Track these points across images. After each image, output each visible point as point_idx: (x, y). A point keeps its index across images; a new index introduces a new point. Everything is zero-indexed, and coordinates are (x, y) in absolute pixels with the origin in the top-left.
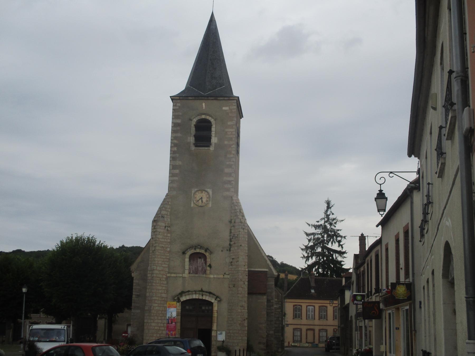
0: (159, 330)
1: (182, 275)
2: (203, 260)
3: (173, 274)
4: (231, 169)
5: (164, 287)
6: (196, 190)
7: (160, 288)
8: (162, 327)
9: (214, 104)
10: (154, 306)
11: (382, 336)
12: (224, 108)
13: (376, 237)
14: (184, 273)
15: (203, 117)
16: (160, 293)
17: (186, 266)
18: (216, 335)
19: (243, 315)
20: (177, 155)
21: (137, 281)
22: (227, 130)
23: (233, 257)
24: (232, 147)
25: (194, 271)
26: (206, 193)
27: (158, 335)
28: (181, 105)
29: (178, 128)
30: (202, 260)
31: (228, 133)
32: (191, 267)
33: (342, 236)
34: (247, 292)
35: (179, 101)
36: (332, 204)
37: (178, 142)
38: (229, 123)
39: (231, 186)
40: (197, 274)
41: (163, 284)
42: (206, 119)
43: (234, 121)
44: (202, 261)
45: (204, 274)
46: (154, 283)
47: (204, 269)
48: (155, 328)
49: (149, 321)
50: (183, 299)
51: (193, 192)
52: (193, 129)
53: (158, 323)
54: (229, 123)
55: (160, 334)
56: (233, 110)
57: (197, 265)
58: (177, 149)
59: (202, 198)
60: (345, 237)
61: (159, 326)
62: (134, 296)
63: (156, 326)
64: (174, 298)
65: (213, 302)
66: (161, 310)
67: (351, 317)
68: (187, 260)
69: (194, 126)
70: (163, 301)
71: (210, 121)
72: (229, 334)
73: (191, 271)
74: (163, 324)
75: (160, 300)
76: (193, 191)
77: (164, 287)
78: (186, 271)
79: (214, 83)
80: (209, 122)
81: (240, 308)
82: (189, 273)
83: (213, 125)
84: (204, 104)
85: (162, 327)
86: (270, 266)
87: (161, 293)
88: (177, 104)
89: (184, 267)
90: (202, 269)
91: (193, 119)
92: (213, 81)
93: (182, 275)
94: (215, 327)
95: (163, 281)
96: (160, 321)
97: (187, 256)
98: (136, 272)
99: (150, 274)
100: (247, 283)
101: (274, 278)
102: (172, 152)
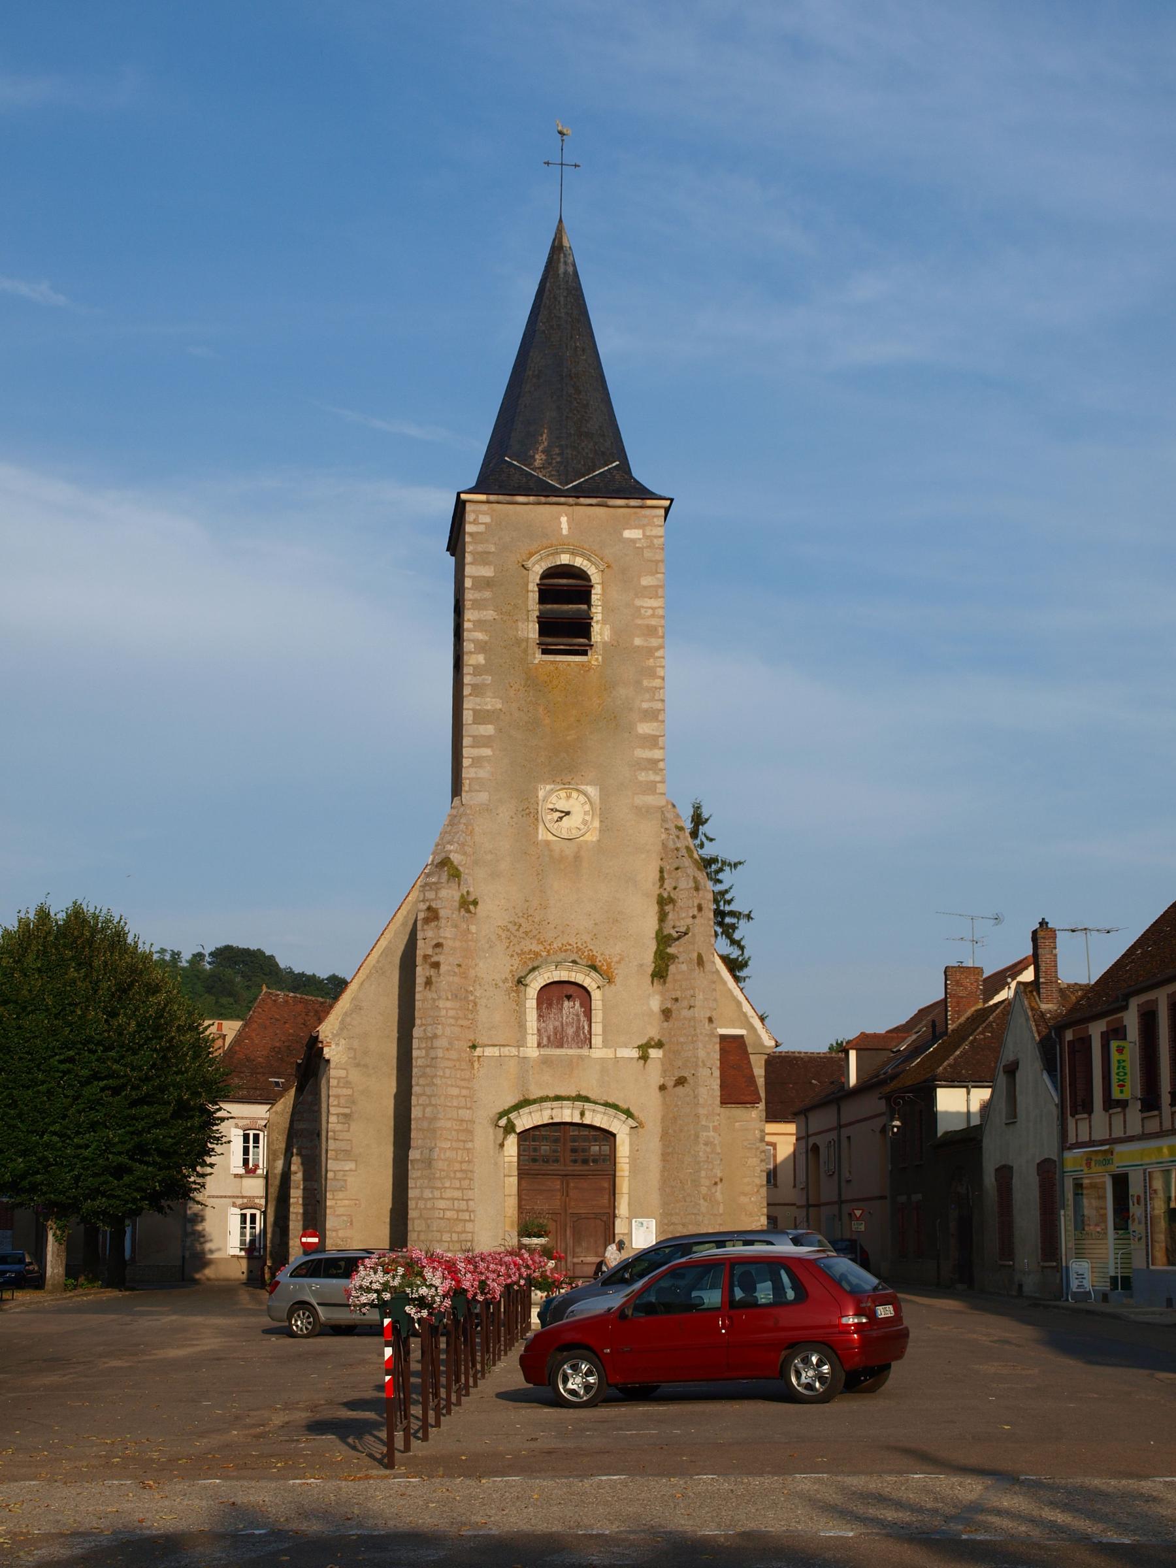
1: (519, 1052)
2: (577, 1004)
4: (655, 724)
5: (463, 1088)
6: (548, 787)
7: (455, 1091)
8: (463, 1211)
9: (592, 513)
10: (441, 1149)
11: (655, 1270)
12: (628, 534)
13: (1108, 932)
14: (521, 1043)
15: (565, 559)
16: (455, 1107)
17: (529, 1024)
18: (626, 1231)
19: (712, 1170)
20: (488, 679)
21: (342, 1073)
22: (638, 602)
23: (678, 994)
24: (657, 654)
25: (552, 1038)
26: (582, 798)
27: (453, 1234)
28: (492, 521)
29: (487, 594)
30: (574, 1004)
31: (643, 611)
32: (543, 1025)
33: (740, 913)
34: (719, 1099)
35: (485, 507)
37: (486, 638)
38: (646, 581)
39: (658, 778)
41: (462, 1080)
42: (573, 566)
43: (659, 576)
44: (576, 1007)
45: (582, 1048)
46: (439, 1076)
47: (584, 1032)
48: (446, 1217)
49: (427, 1194)
50: (525, 1120)
51: (541, 794)
52: (534, 596)
53: (453, 1199)
54: (646, 581)
55: (458, 1233)
56: (655, 541)
57: (560, 1019)
58: (485, 659)
59: (568, 813)
60: (749, 917)
61: (456, 1208)
62: (332, 1119)
63: (448, 1210)
64: (497, 1122)
67: (1005, 1173)
68: (531, 1004)
69: (536, 589)
70: (463, 1131)
71: (587, 574)
73: (543, 1038)
74: (465, 1202)
75: (455, 1130)
76: (543, 790)
77: (463, 1088)
78: (529, 1037)
79: (587, 454)
80: (581, 575)
81: (703, 1147)
82: (539, 1045)
83: (596, 585)
84: (566, 518)
85: (463, 1211)
86: (752, 1020)
87: (458, 1108)
88: (480, 516)
89: (522, 1026)
90: (577, 1033)
91: (534, 565)
92: (583, 445)
93: (519, 1052)
94: (623, 1208)
95: (462, 1070)
96: (458, 1194)
97: (533, 991)
98: (337, 1044)
99: (424, 1051)
100: (717, 1073)
101: (766, 1056)
102: (472, 668)
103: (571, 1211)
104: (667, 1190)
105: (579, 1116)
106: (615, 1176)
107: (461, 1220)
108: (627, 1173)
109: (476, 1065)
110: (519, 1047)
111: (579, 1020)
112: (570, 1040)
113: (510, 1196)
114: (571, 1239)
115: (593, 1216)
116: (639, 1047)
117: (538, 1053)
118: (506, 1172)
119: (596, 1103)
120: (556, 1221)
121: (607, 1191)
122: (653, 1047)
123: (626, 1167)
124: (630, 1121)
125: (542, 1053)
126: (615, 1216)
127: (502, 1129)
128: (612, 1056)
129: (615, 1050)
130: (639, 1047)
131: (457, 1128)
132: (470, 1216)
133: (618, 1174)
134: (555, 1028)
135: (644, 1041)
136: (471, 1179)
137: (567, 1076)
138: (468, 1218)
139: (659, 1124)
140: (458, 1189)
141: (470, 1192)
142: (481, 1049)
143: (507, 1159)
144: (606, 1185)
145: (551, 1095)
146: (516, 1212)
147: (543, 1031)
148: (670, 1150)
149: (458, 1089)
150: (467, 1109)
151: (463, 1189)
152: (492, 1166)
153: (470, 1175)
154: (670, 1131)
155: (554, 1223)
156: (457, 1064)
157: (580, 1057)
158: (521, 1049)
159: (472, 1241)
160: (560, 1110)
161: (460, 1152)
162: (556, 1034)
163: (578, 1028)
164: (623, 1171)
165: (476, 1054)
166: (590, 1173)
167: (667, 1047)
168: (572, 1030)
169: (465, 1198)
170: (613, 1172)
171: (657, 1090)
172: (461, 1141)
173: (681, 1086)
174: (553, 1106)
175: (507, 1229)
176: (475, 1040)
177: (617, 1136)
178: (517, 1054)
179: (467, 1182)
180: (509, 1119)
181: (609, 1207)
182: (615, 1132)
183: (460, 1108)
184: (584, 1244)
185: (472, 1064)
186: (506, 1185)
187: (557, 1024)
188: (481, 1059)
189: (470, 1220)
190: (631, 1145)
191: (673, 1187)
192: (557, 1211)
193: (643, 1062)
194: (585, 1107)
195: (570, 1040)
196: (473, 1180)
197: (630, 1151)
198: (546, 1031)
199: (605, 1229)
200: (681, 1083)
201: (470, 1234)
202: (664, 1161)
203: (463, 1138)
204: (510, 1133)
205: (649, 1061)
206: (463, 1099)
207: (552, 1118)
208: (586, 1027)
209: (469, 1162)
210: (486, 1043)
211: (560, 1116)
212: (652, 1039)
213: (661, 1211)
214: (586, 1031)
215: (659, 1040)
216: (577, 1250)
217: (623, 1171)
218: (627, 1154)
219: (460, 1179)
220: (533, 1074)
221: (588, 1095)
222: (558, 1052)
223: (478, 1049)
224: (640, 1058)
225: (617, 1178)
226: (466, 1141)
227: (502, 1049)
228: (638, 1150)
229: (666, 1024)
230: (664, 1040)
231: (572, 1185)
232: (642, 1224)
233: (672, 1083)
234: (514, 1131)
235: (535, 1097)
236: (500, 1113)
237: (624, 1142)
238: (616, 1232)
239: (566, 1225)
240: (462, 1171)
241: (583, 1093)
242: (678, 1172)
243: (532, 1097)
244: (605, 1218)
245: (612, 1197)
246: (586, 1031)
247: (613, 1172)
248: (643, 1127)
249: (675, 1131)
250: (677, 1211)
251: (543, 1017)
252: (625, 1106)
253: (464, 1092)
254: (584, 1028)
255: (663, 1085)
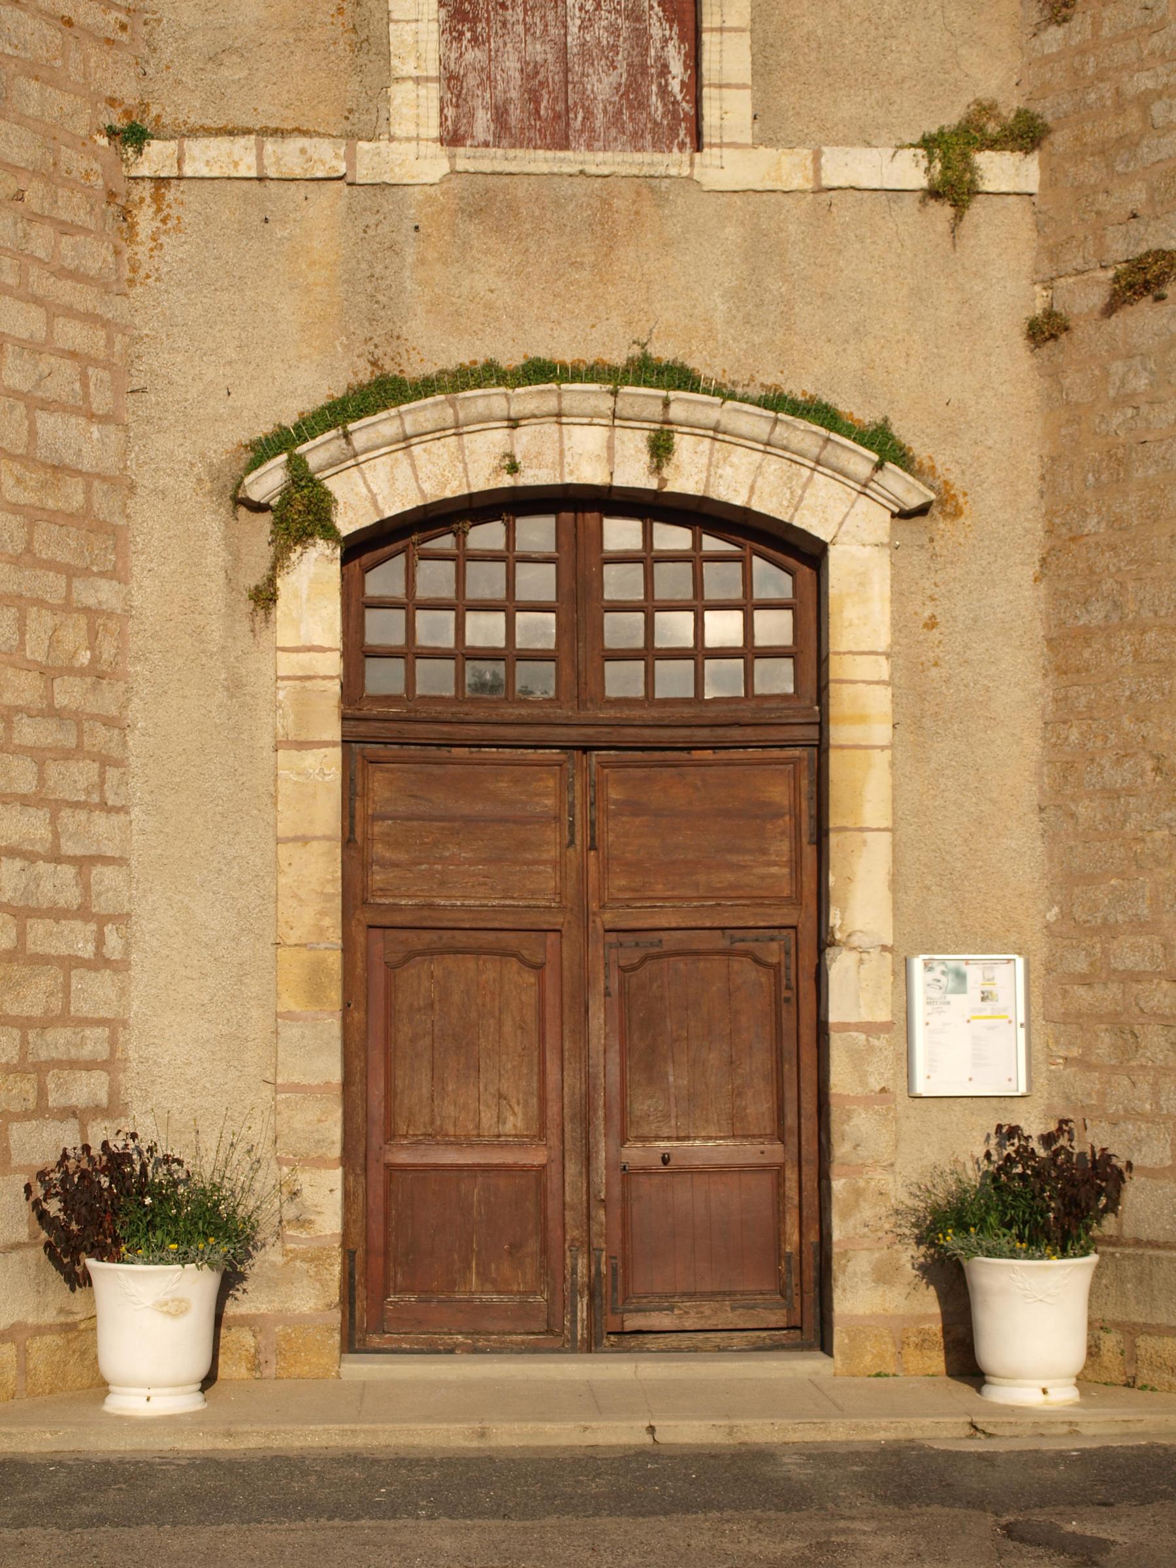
0: (70, 573)
1: (351, 158)
3: (218, 147)
5: (70, 312)
8: (58, 914)
17: (400, 35)
18: (883, 1015)
25: (515, 115)
32: (473, 55)
36: (940, 525)
40: (563, 144)
47: (664, 91)
55: (24, 1024)
57: (553, 31)
65: (828, 541)
66: (35, 650)
72: (1108, 996)
74: (68, 872)
77: (70, 312)
78: (401, 94)
82: (453, 138)
85: (58, 914)
95: (66, 229)
103: (608, 918)
104: (1082, 810)
105: (646, 458)
106: (821, 747)
107: (44, 960)
108: (881, 733)
109: (145, 221)
110: (352, 137)
111: (641, 37)
112: (599, 121)
113: (304, 840)
114: (614, 1057)
115: (720, 942)
116: (928, 143)
117: (446, 168)
118: (286, 724)
119: (725, 393)
120: (538, 967)
121: (786, 822)
122: (993, 144)
123: (879, 701)
124: (896, 482)
125: (461, 165)
126: (823, 941)
127: (265, 521)
128: (799, 180)
129: (817, 156)
130: (928, 143)
131: (26, 497)
132: (100, 941)
133: (838, 734)
134: (530, 72)
135: (951, 117)
136: (105, 761)
137: (585, 275)
138: (87, 951)
139: (1032, 497)
140: (25, 801)
141: (101, 823)
142: (173, 145)
143: (288, 664)
144: (778, 793)
145: (511, 358)
146: (332, 924)
147: (472, 80)
148: (1097, 614)
149: (37, 315)
150: (91, 416)
151: (56, 807)
152: (221, 696)
153: (100, 737)
154: (1091, 524)
155: (530, 978)
156: (35, 192)
157: (647, 183)
158: (363, 145)
159: (110, 1065)
160: (551, 428)
161: (40, 623)
162: (533, 97)
163: (638, 71)
164: (862, 719)
165: (144, 170)
166: (703, 734)
167: (1060, 140)
168: (613, 78)
169: (69, 848)
170: (813, 732)
171: (1019, 343)
172: (52, 565)
173: (1146, 303)
174: (516, 410)
175: (288, 1003)
176: (145, 106)
177: (833, 554)
178: (342, 169)
179: (83, 773)
180: (297, 466)
181: (796, 900)
182: (823, 534)
183: (46, 405)
184: (676, 1078)
185: (125, 213)
186: (284, 788)
187: (538, 51)
188: (170, 195)
189: (100, 962)
190: (899, 596)
191: (1112, 794)
192: (545, 920)
193: (948, 211)
194: (677, 412)
195: (599, 121)
196: (118, 763)
197: (897, 627)
198: (488, 80)
199: (778, 1002)
200: (1147, 286)
201: (102, 1032)
202: (1061, 671)
203: (64, 557)
204: (303, 537)
205: (977, 209)
206: (69, 369)
207: (513, 469)
208: (677, 68)
209: (97, 674)
210: (194, 120)
211: (550, 456)
212: (987, 109)
213: (1052, 914)
214: (675, 86)
215: (1019, 114)
216: (641, 1105)
217: (862, 719)
218: (883, 640)
219: (39, 756)
220: (422, 261)
221: (691, 364)
222: (541, 161)
223: (154, 148)
224: (934, 193)
225: (834, 757)
226: (86, 572)
227: (270, 145)
228: (931, 624)
229: (1054, 36)
230: (1046, 110)
231: (614, 793)
232: (960, 977)
233: (1098, 297)
234: (329, 532)
235: (431, 370)
236: (253, 446)
237: (863, 582)
238: (833, 1018)
239: (584, 985)
240: (52, 712)
241: (663, 351)
242: (1139, 720)
243: (415, 369)
244: (773, 953)
245: (809, 852)
246: (675, 86)
247: (813, 732)
248: (957, 513)
249: (1117, 523)
250: (1144, 910)
251: (475, 20)
252: (866, 415)
253: (72, 334)
254: (664, 70)
255: (1050, 314)
